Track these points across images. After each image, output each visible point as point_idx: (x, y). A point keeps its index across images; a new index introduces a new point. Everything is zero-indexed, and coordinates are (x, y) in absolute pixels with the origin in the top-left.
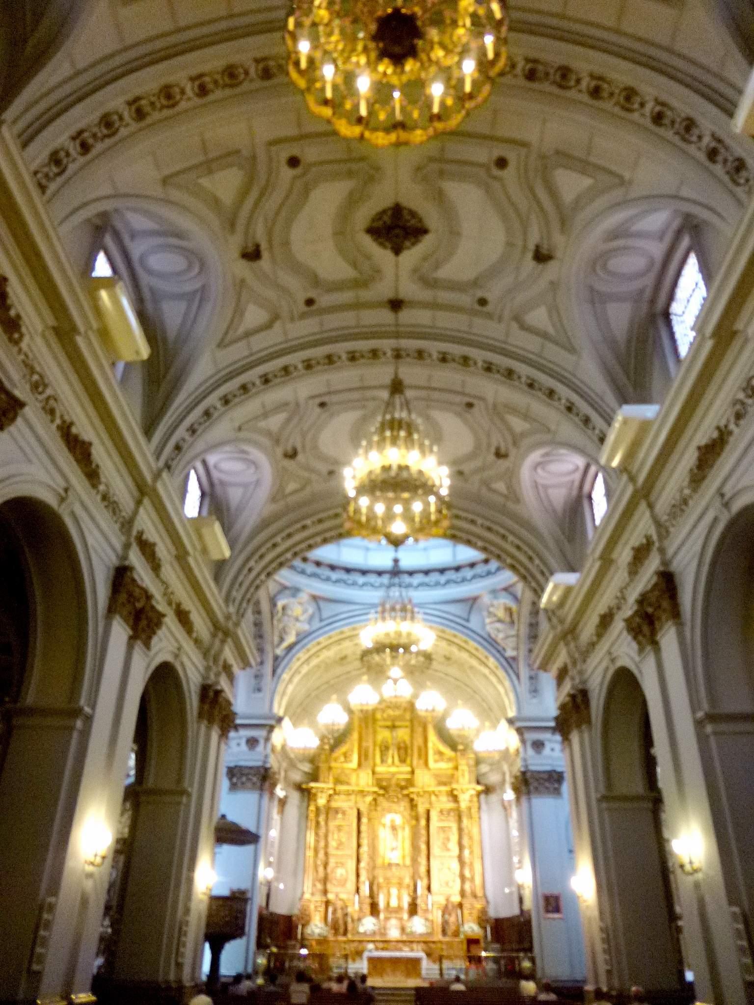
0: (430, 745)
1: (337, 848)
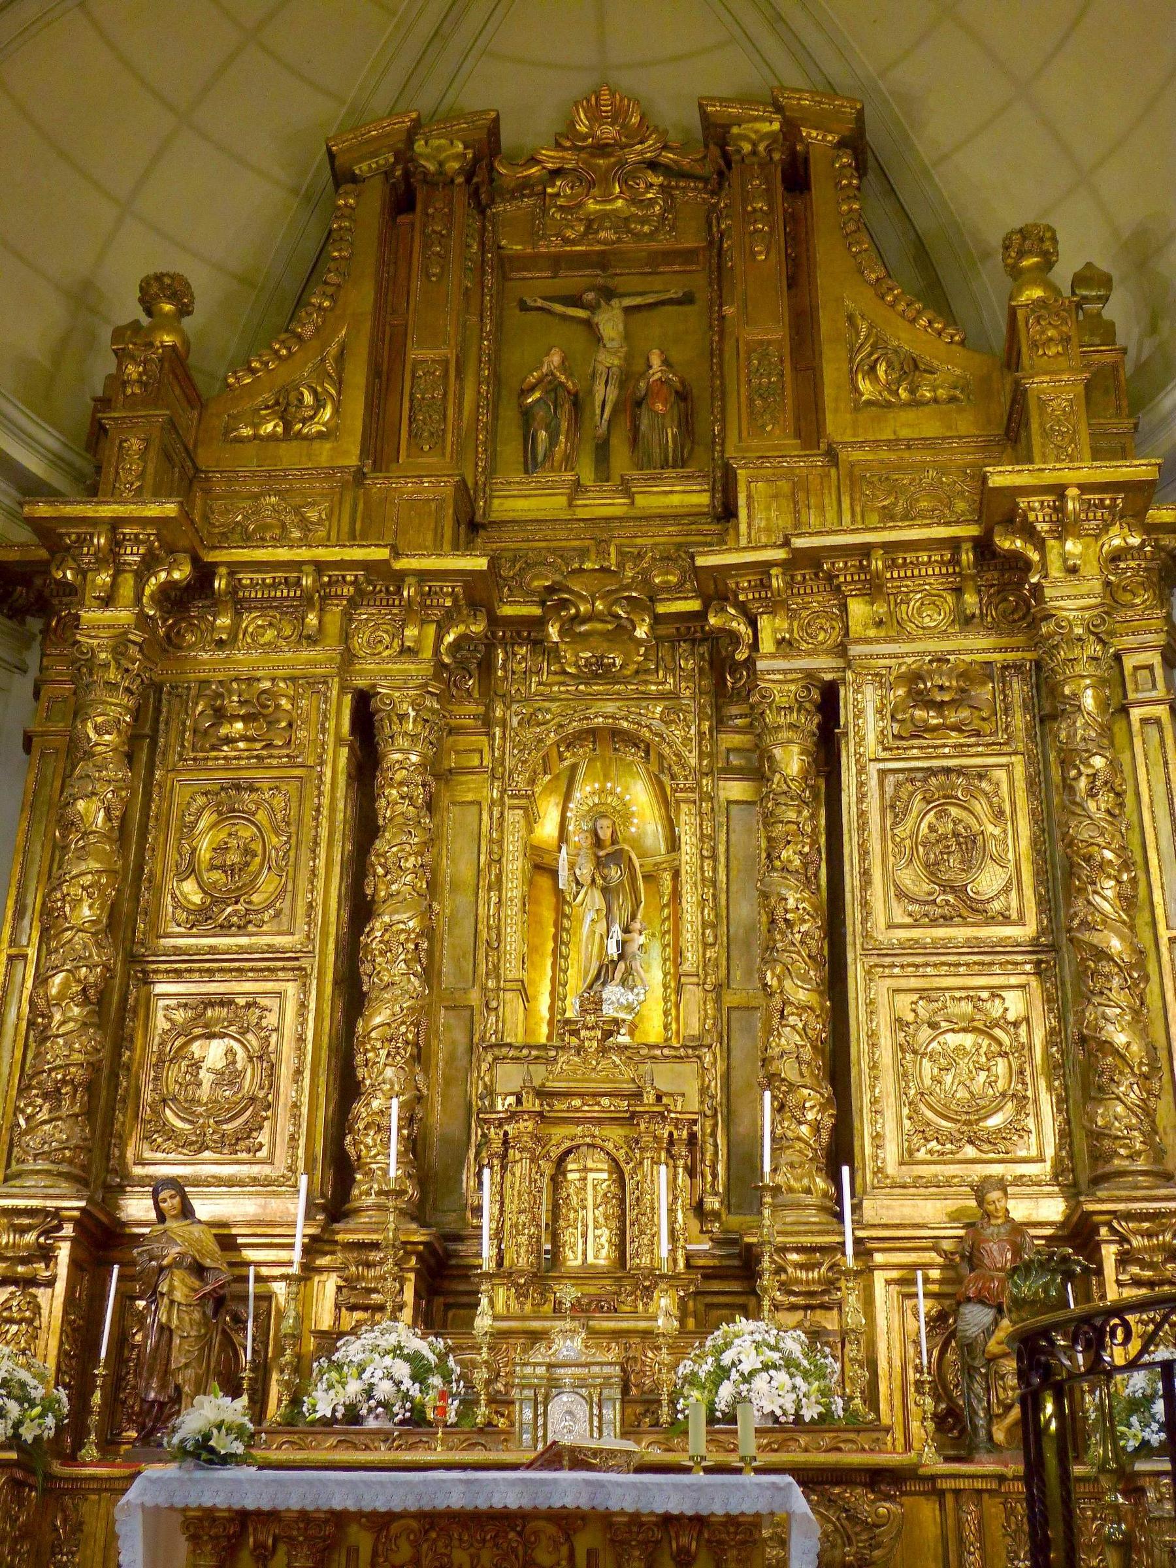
1: (201, 918)
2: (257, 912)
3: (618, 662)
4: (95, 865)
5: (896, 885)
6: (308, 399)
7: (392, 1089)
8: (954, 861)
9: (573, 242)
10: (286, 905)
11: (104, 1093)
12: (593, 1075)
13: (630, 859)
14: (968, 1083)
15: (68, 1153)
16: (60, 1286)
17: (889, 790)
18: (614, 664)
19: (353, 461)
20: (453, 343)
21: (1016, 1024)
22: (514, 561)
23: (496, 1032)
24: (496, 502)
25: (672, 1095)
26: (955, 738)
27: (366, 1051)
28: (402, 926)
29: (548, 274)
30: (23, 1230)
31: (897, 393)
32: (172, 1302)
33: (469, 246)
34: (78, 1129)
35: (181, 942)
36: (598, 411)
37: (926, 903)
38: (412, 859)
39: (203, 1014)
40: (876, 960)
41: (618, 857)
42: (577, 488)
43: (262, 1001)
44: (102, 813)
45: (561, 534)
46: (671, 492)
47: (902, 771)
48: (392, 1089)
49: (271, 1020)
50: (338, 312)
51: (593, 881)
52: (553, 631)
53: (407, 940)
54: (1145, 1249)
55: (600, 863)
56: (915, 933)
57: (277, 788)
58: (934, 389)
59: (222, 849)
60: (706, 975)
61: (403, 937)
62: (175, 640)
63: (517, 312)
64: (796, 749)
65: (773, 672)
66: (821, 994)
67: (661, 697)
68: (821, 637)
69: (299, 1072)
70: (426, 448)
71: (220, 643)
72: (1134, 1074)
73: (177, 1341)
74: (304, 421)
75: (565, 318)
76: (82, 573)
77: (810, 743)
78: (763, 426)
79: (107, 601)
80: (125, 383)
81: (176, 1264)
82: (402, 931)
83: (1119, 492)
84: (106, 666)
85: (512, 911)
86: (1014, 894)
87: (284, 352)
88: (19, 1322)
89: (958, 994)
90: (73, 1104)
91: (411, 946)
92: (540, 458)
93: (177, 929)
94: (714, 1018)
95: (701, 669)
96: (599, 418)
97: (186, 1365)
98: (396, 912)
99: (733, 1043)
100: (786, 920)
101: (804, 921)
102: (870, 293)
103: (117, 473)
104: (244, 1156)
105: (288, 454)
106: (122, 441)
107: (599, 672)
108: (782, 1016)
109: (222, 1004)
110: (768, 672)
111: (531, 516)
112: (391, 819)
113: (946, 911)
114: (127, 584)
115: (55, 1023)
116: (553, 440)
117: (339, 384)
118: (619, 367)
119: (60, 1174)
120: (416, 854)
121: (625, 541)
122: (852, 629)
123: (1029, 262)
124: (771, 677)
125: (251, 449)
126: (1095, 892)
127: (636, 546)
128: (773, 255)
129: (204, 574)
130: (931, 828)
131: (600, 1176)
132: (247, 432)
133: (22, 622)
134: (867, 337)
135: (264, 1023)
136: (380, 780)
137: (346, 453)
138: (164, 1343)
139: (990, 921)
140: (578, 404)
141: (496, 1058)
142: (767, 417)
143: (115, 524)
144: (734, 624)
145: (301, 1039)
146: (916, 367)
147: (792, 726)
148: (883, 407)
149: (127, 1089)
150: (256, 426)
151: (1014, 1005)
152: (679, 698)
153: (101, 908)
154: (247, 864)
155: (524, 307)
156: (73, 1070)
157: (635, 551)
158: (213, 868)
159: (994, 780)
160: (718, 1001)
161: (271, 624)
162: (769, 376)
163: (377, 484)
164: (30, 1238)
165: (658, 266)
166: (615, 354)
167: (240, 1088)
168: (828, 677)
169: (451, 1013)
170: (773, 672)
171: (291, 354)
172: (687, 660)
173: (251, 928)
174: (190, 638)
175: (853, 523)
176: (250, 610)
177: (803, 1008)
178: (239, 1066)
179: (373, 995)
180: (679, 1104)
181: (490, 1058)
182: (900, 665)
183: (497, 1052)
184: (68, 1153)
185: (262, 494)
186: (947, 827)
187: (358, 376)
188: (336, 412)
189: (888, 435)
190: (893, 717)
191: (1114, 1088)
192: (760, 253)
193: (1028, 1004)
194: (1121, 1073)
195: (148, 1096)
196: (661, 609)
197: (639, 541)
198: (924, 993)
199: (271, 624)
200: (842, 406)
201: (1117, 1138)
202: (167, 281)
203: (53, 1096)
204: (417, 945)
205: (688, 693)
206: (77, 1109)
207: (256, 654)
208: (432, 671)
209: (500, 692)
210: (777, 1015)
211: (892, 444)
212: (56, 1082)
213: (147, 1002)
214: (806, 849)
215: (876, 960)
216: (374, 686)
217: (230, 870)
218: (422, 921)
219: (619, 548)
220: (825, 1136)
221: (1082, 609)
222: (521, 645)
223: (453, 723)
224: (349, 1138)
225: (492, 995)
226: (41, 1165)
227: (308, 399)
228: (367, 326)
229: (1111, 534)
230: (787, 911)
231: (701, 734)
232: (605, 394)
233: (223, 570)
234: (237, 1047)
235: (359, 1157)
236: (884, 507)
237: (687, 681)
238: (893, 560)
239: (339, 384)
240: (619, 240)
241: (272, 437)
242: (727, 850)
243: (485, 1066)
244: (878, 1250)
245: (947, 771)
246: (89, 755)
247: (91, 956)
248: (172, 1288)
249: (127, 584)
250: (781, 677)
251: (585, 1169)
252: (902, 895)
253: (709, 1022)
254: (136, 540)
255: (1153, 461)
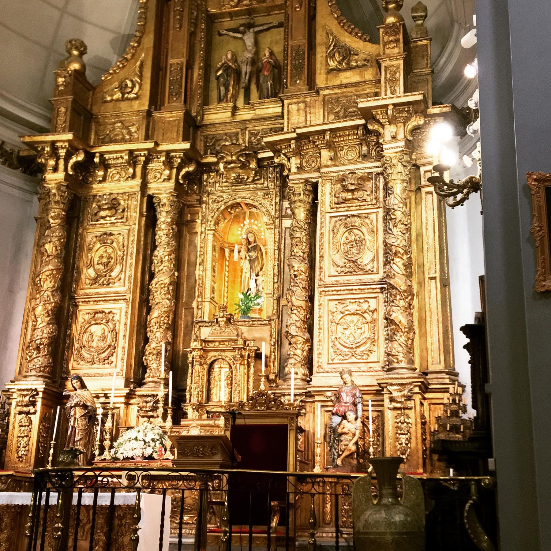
0: (320, 37)
1: (95, 281)
2: (112, 279)
3: (246, 177)
4: (51, 267)
5: (333, 261)
6: (129, 84)
7: (157, 340)
8: (354, 250)
9: (234, 7)
10: (122, 276)
11: (61, 346)
12: (223, 334)
13: (260, 248)
14: (353, 333)
15: (42, 369)
16: (38, 414)
17: (333, 224)
18: (244, 178)
19: (146, 108)
20: (185, 56)
21: (373, 312)
22: (212, 139)
23: (201, 317)
24: (205, 116)
25: (250, 340)
26: (357, 203)
27: (150, 327)
28: (162, 282)
29: (229, 19)
30: (25, 396)
31: (342, 64)
32: (75, 418)
33: (193, 13)
34: (46, 360)
35: (87, 291)
36: (244, 76)
37: (343, 267)
38: (167, 257)
39: (94, 316)
40: (323, 289)
41: (255, 248)
42: (235, 109)
43: (114, 311)
44: (54, 248)
45: (229, 128)
46: (269, 108)
47: (337, 216)
48: (157, 340)
49: (117, 318)
50: (141, 47)
51: (246, 258)
52: (221, 166)
53: (165, 287)
54: (398, 396)
55: (248, 251)
56: (341, 279)
57: (120, 234)
58: (357, 62)
59: (101, 257)
60: (274, 293)
61: (163, 286)
62: (86, 181)
63: (217, 36)
64: (302, 209)
65: (295, 180)
66: (306, 301)
67: (263, 189)
68: (313, 164)
69: (125, 336)
70: (175, 99)
71: (100, 182)
72: (402, 332)
73: (77, 431)
74: (129, 93)
75: (235, 38)
76: (46, 160)
77: (308, 207)
78: (296, 81)
79: (55, 169)
80: (58, 86)
81: (77, 405)
82: (162, 284)
83: (410, 105)
84: (54, 195)
85: (209, 272)
86: (375, 262)
87: (121, 66)
88: (25, 426)
89: (352, 301)
90: (44, 351)
91: (166, 289)
92: (222, 98)
93: (86, 286)
94: (277, 309)
95: (277, 177)
96: (245, 79)
97: (81, 439)
98: (161, 277)
99: (283, 318)
100: (294, 275)
101: (301, 275)
102: (336, 22)
103: (57, 121)
104: (107, 365)
105: (124, 105)
106: (58, 109)
107: (239, 181)
108: (292, 310)
109: (100, 312)
110: (293, 180)
111: (217, 121)
112: (160, 243)
113: (350, 270)
114: (61, 163)
115: (38, 324)
116: (227, 90)
117: (141, 77)
118: (251, 58)
119: (39, 376)
120: (168, 255)
121: (252, 129)
122: (322, 162)
123: (391, 6)
124: (295, 182)
125: (110, 105)
126: (394, 263)
127: (255, 130)
128: (303, 8)
129: (90, 156)
130: (347, 239)
131: (225, 371)
132: (109, 99)
133: (36, 176)
134: (332, 42)
135: (114, 318)
136: (157, 229)
137: (144, 105)
138: (73, 432)
139: (367, 273)
140: (238, 73)
141: (200, 327)
142: (297, 77)
143: (53, 143)
144: (284, 161)
145: (126, 324)
146: (350, 53)
147: (300, 201)
148: (338, 71)
149: (69, 344)
150: (112, 96)
151: (373, 304)
152: (269, 189)
153: (55, 282)
154: (110, 262)
155: (220, 35)
156: (43, 340)
157: (255, 132)
158: (98, 264)
159: (371, 219)
160: (278, 303)
161: (118, 173)
162: (298, 60)
163: (157, 115)
164: (27, 398)
165: (270, 12)
166: (250, 52)
167: (106, 342)
168: (314, 181)
169: (187, 310)
170: (295, 180)
171: (124, 66)
172: (272, 174)
173: (111, 285)
174: (91, 179)
175: (386, 95)
176: (110, 168)
177: (299, 307)
178: (106, 334)
179: (153, 307)
180: (252, 343)
181: (198, 326)
182: (338, 175)
183: (200, 324)
184: (42, 369)
185: (115, 123)
186: (352, 238)
187: (148, 73)
188: (140, 88)
189: (338, 83)
190: (335, 196)
191: (395, 337)
192: (298, 7)
193: (378, 303)
194: (398, 331)
195: (76, 345)
196: (260, 156)
197: (256, 128)
198: (340, 301)
199: (118, 173)
200: (322, 71)
201: (393, 355)
202: (74, 42)
203: (38, 349)
204: (168, 288)
205: (272, 186)
206: (46, 353)
207: (112, 184)
208: (173, 188)
209: (205, 191)
210: (290, 310)
211: (340, 87)
212: (37, 344)
213: (75, 314)
214: (304, 247)
215: (323, 289)
216: (153, 194)
217: (106, 265)
218: (170, 279)
219: (249, 131)
220: (305, 353)
221: (396, 153)
222: (212, 172)
223: (188, 203)
224: (144, 358)
225: (200, 303)
226: (33, 373)
227: (129, 84)
228: (151, 53)
229: (411, 120)
230: (294, 271)
231: (276, 203)
232: (246, 69)
233: (98, 155)
234: (105, 328)
235: (147, 364)
236: (336, 112)
237: (272, 182)
238: (336, 135)
239: (141, 77)
240: (252, 4)
241: (118, 100)
242: (284, 246)
243: (196, 329)
244: (316, 395)
245: (354, 216)
246: (49, 227)
247: (50, 299)
248: (75, 414)
249: (61, 163)
250: (298, 182)
251: (220, 367)
252: (335, 264)
253: (275, 311)
254: (62, 148)
255: (421, 92)
